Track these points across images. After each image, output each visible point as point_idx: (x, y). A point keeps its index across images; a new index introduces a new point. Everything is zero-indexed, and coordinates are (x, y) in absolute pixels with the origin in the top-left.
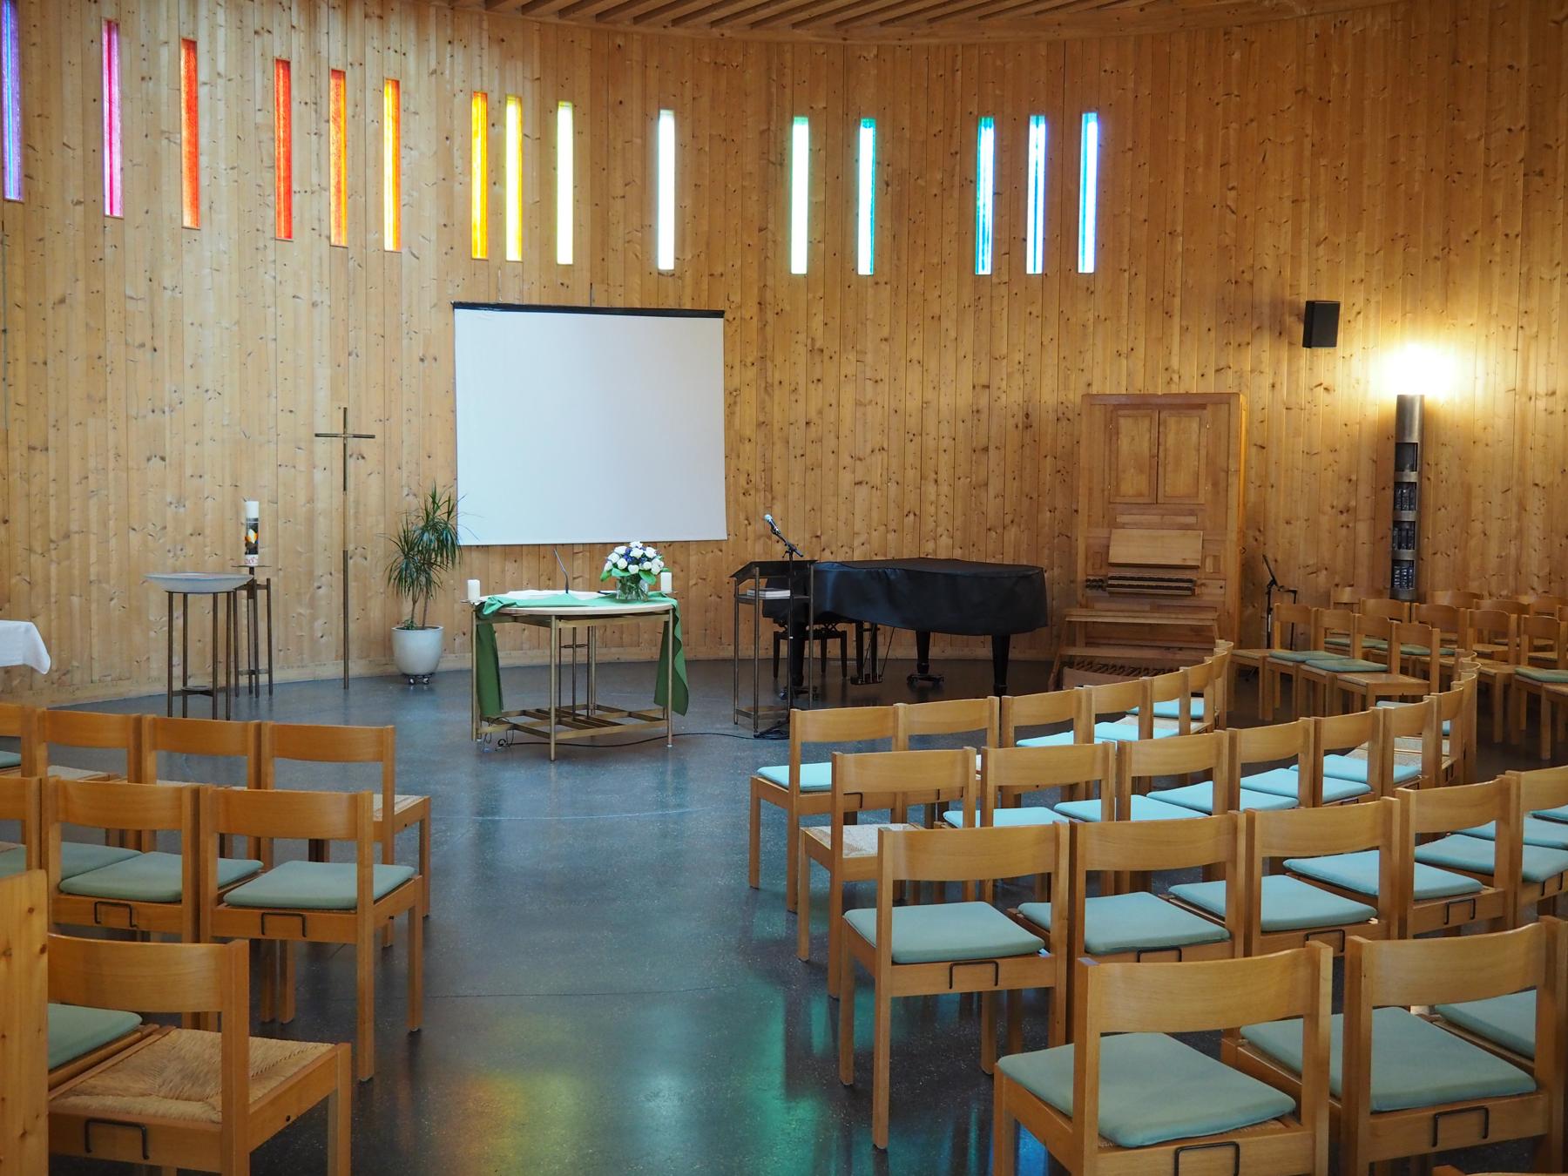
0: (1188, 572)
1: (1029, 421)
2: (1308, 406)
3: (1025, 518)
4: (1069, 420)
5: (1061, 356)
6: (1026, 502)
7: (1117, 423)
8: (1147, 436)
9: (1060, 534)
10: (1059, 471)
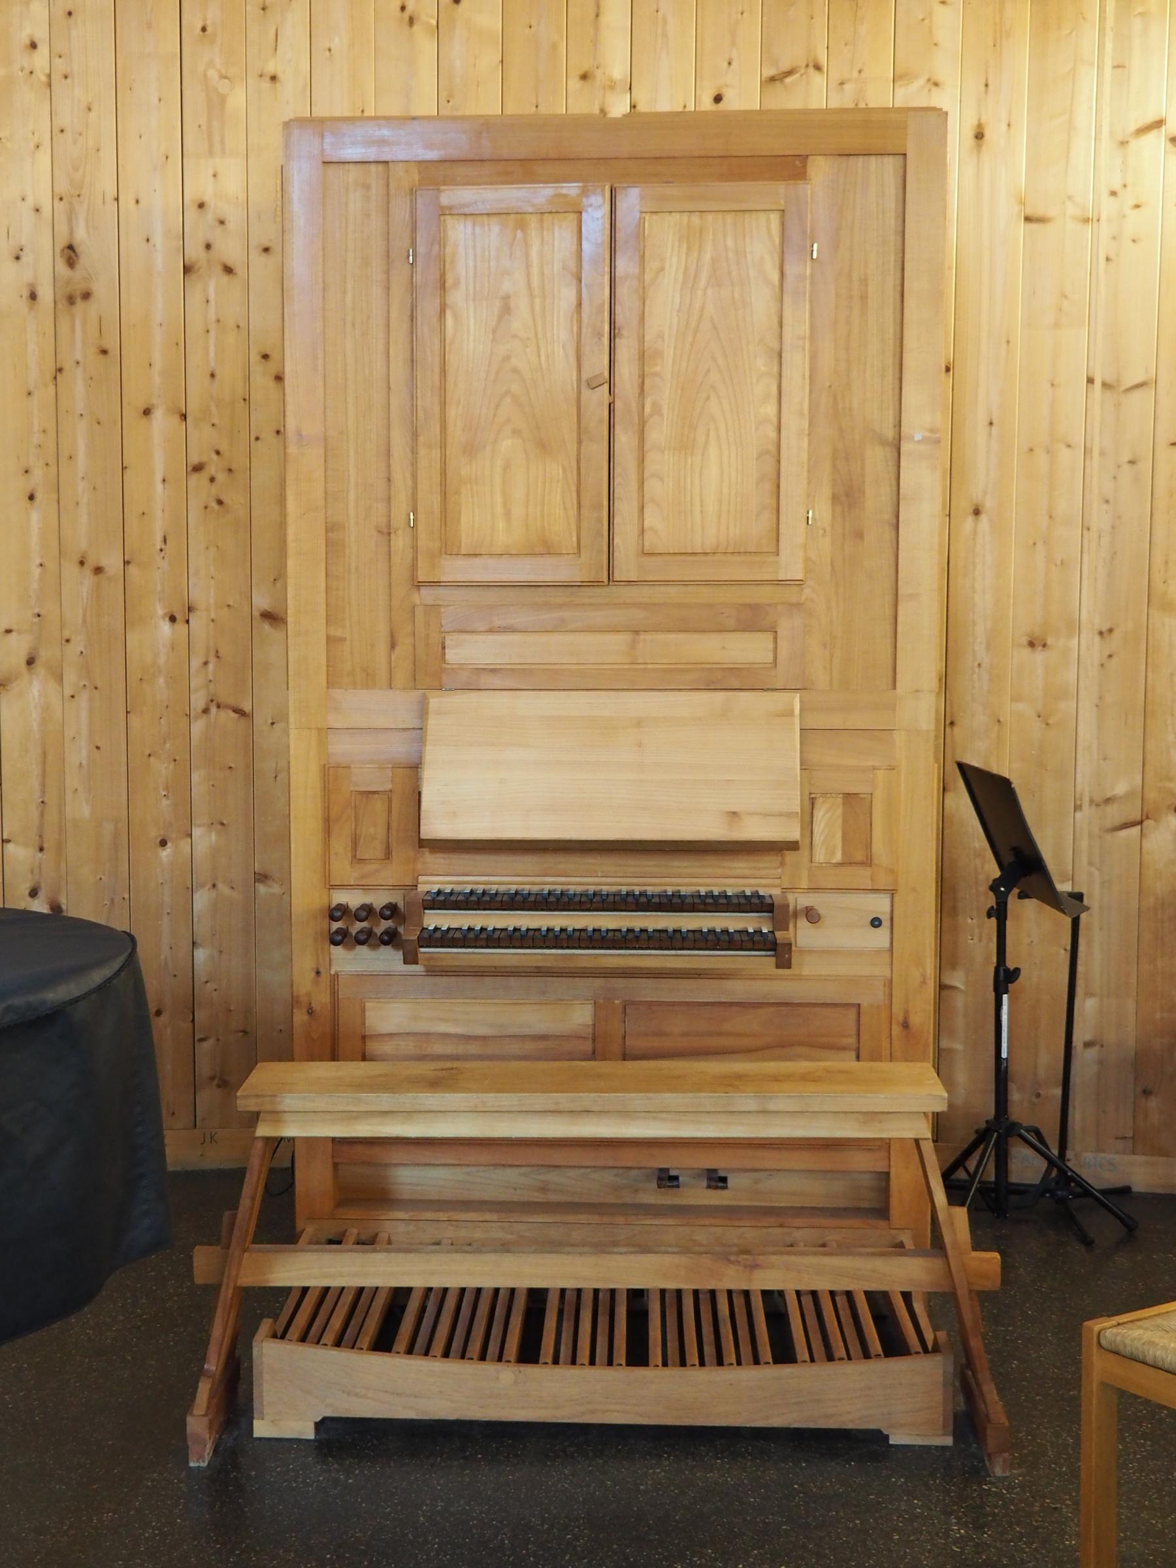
0: (740, 865)
1: (78, 273)
2: (1108, 207)
3: (78, 645)
4: (228, 270)
5: (193, 22)
6: (79, 585)
7: (440, 240)
8: (567, 295)
9: (214, 703)
10: (198, 468)
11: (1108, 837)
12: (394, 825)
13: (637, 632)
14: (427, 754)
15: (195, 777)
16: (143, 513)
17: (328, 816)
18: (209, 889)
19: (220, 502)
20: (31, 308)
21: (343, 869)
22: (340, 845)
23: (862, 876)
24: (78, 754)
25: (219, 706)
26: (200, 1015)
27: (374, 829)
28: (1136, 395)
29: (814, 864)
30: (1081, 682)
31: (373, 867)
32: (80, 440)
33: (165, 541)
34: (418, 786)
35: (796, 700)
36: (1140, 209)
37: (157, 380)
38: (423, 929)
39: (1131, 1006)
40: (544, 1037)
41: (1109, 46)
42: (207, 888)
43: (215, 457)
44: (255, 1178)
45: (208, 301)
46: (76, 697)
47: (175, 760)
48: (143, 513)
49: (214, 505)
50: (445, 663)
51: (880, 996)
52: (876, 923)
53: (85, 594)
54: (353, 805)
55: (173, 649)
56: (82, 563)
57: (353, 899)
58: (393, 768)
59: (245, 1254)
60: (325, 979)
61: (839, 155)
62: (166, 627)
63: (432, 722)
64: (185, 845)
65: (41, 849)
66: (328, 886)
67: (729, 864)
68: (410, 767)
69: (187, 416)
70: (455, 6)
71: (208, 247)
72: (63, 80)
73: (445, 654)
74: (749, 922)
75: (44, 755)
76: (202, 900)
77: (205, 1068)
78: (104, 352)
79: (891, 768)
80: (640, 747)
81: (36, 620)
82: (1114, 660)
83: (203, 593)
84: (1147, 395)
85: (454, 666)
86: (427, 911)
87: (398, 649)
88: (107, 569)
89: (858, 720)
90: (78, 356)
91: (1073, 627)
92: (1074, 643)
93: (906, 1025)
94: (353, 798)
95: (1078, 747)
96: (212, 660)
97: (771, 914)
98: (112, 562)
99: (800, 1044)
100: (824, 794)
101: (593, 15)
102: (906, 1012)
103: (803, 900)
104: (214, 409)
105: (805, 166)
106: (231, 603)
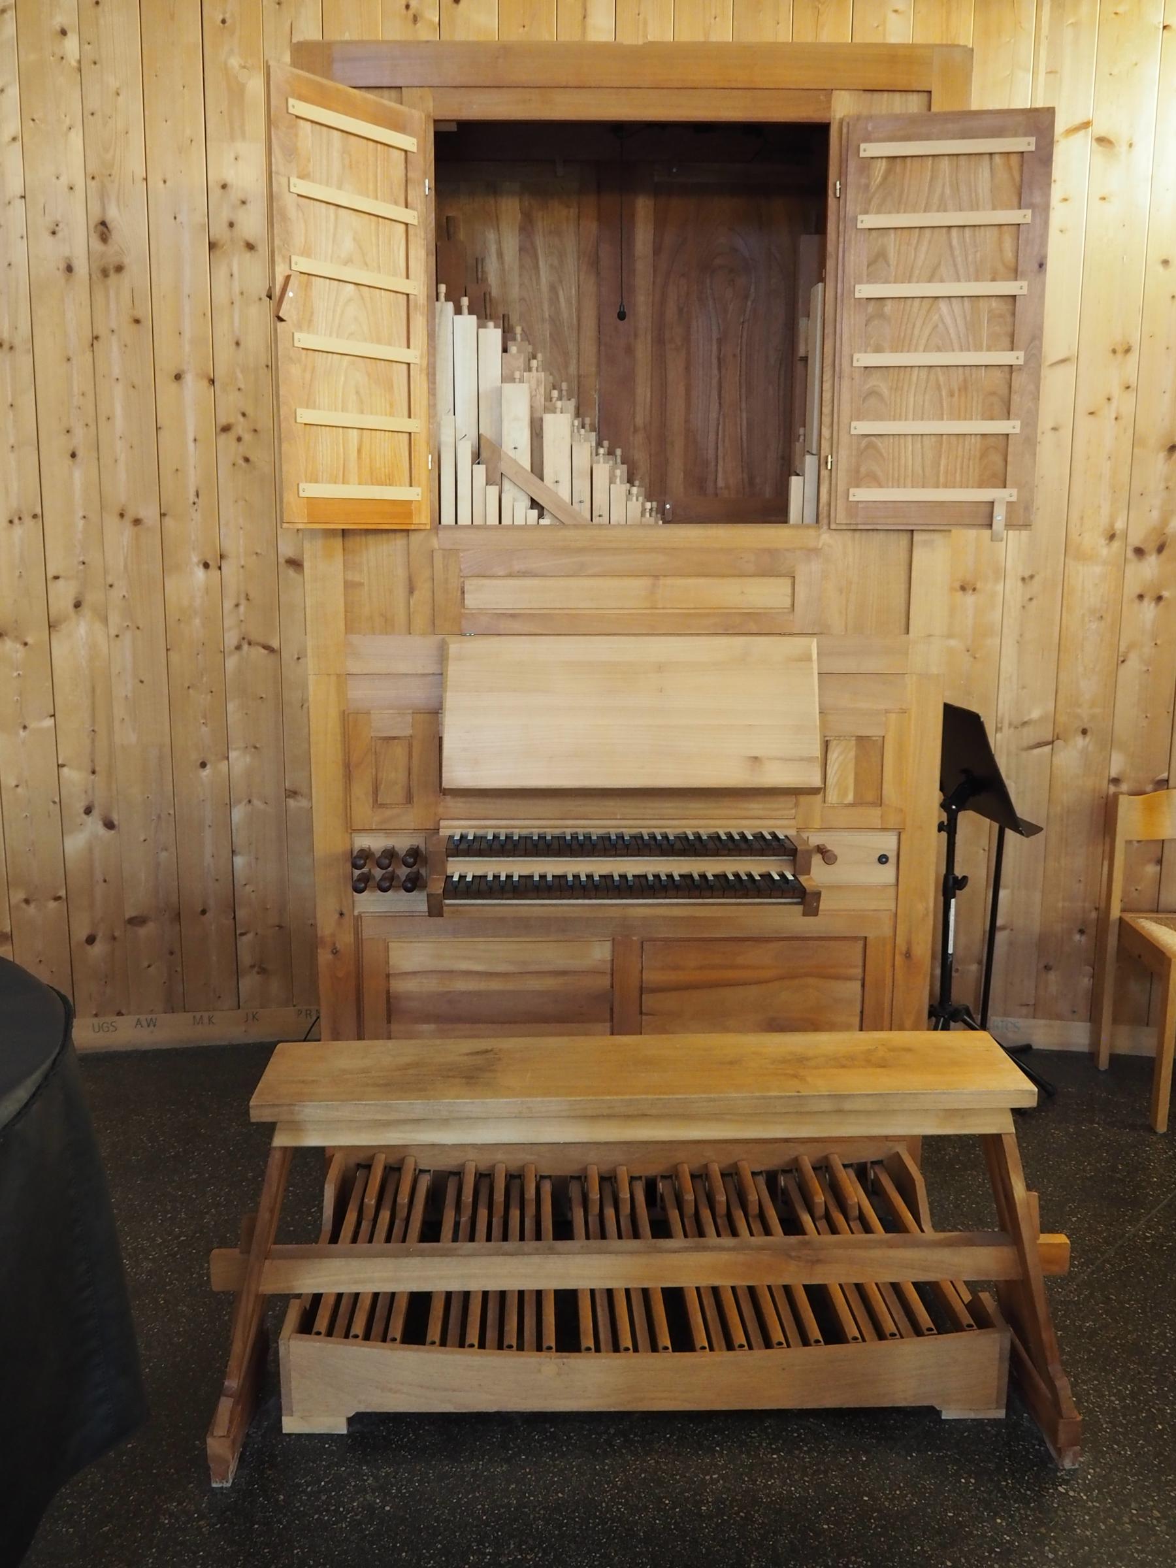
0: (756, 807)
1: (111, 249)
5: (214, 15)
6: (119, 536)
9: (246, 641)
10: (226, 429)
11: (1024, 754)
12: (415, 770)
13: (656, 577)
14: (447, 700)
15: (231, 707)
16: (177, 470)
17: (349, 761)
18: (245, 805)
19: (247, 460)
20: (67, 280)
21: (363, 811)
22: (361, 790)
23: (873, 816)
24: (124, 688)
25: (250, 644)
26: (241, 913)
27: (394, 775)
28: (1061, 370)
29: (826, 805)
30: (1005, 621)
31: (395, 811)
32: (117, 402)
33: (198, 495)
34: (439, 731)
35: (813, 644)
36: (1068, 202)
37: (187, 348)
38: (447, 877)
39: (1037, 897)
40: (564, 973)
41: (1043, 54)
42: (244, 803)
43: (241, 419)
44: (274, 1189)
45: (232, 275)
46: (121, 637)
47: (212, 692)
48: (177, 470)
49: (241, 462)
50: (464, 607)
51: (887, 931)
52: (884, 860)
53: (125, 544)
54: (373, 750)
55: (207, 593)
56: (122, 515)
57: (375, 843)
58: (413, 713)
59: (267, 1261)
60: (348, 921)
61: (865, 90)
62: (200, 573)
63: (453, 669)
64: (223, 766)
65: (93, 772)
66: (350, 831)
67: (746, 805)
68: (428, 713)
69: (215, 380)
70: (455, 5)
71: (231, 225)
72: (93, 66)
73: (464, 599)
74: (773, 867)
75: (93, 690)
76: (238, 814)
77: (246, 958)
78: (137, 321)
79: (904, 711)
80: (661, 691)
81: (82, 567)
82: (1034, 602)
83: (235, 543)
84: (1070, 369)
85: (474, 611)
86: (450, 859)
87: (416, 593)
88: (145, 521)
89: (872, 664)
90: (114, 326)
91: (1000, 573)
92: (1000, 588)
93: (908, 955)
94: (373, 744)
95: (1001, 677)
96: (243, 602)
97: (792, 858)
98: (149, 514)
99: (811, 975)
100: (838, 738)
101: (580, 17)
102: (909, 943)
103: (815, 840)
104: (240, 376)
105: (829, 101)
106: (259, 551)
